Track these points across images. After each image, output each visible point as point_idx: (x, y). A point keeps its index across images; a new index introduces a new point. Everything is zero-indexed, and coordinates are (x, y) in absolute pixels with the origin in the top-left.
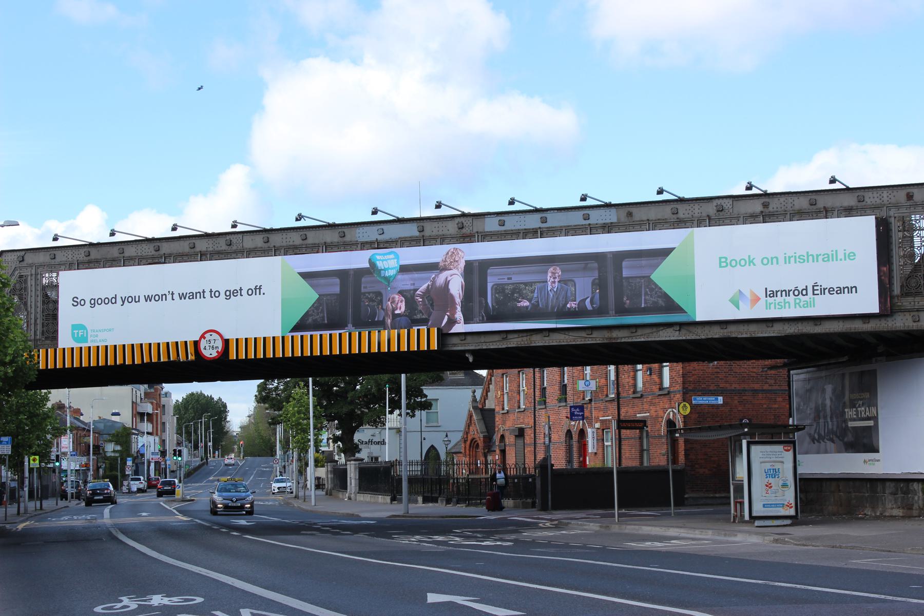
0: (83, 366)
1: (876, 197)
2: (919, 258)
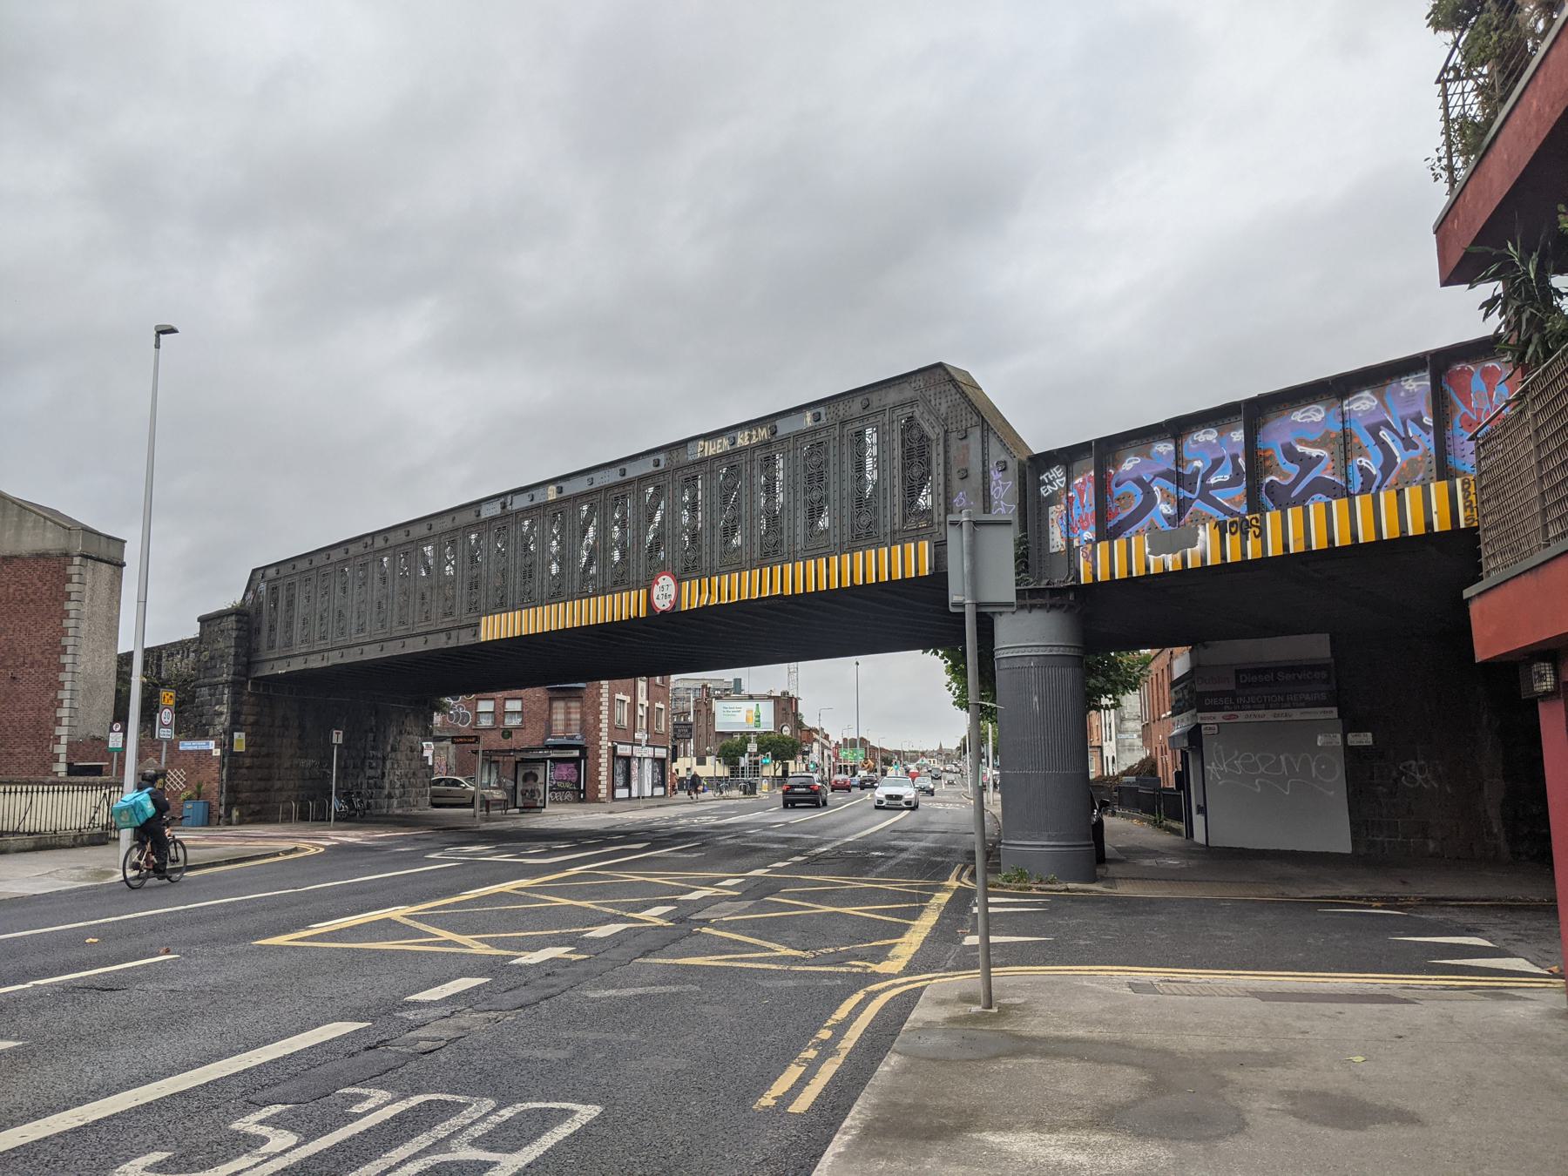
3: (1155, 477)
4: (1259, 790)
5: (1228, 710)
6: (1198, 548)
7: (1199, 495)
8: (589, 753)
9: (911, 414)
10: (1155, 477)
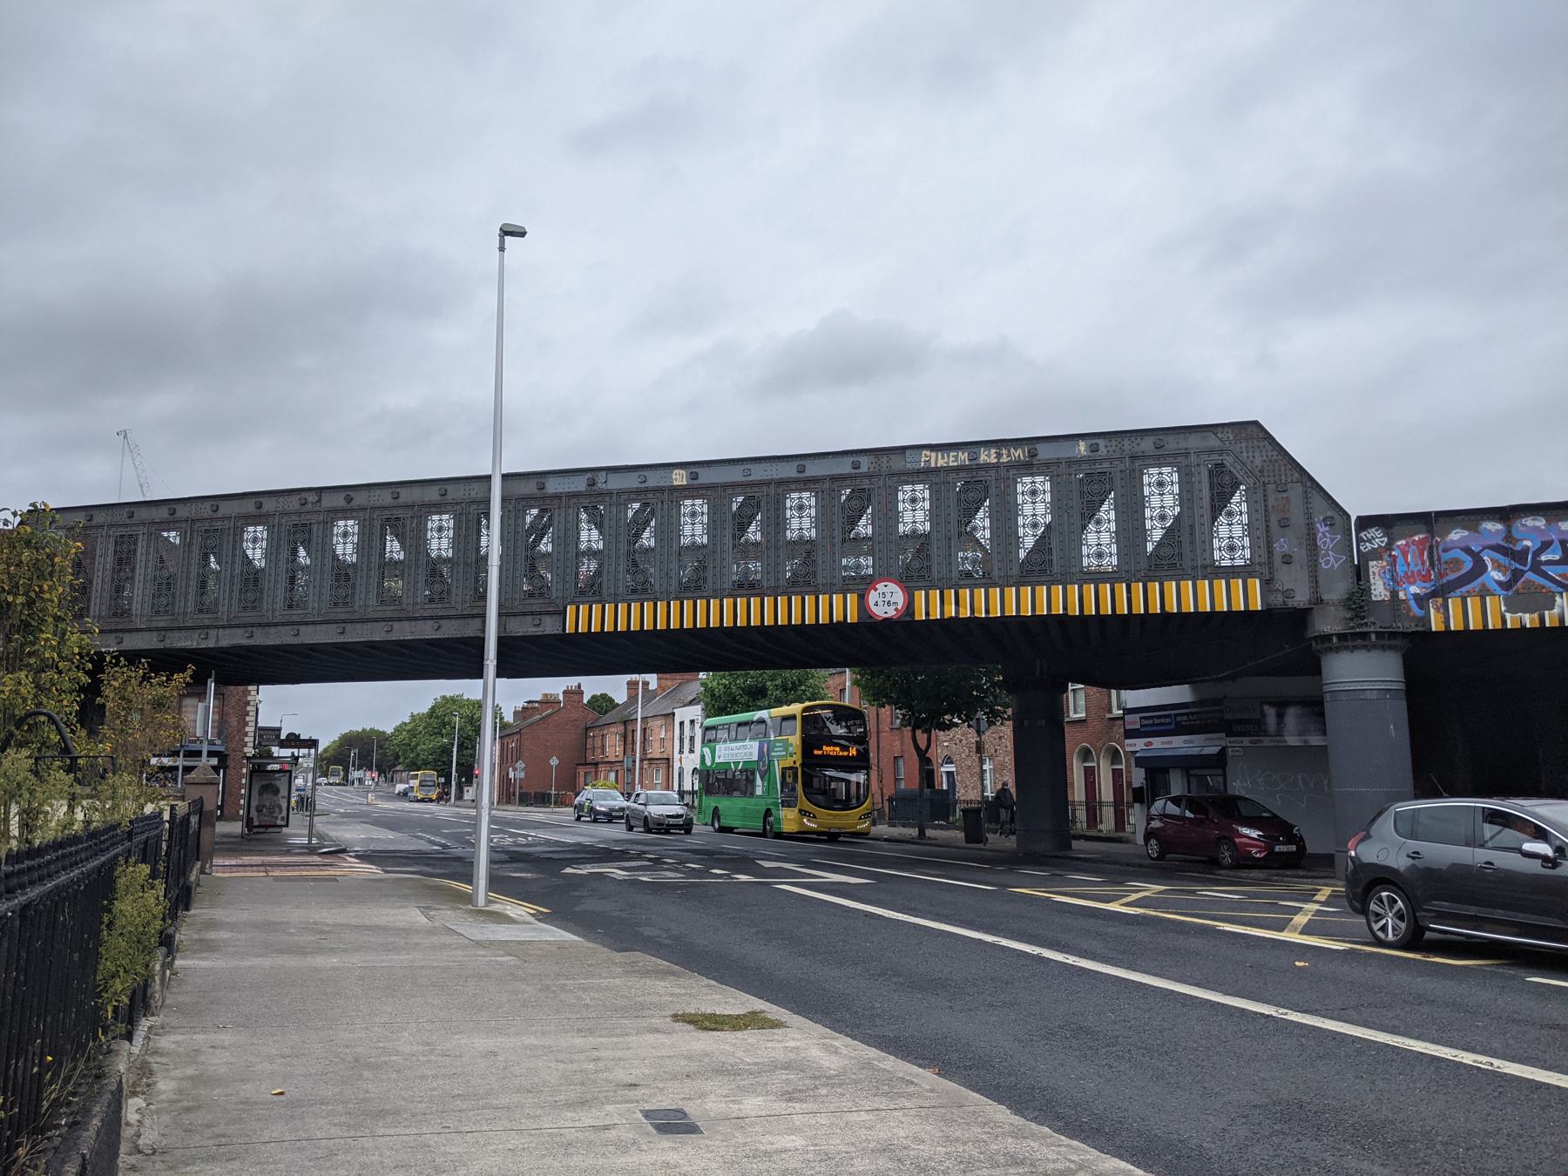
0: (711, 626)
1: (1114, 445)
2: (1172, 521)
3: (1484, 548)
4: (1279, 803)
5: (1253, 736)
6: (1556, 611)
7: (1531, 566)
8: (230, 762)
9: (1220, 462)
10: (1484, 548)
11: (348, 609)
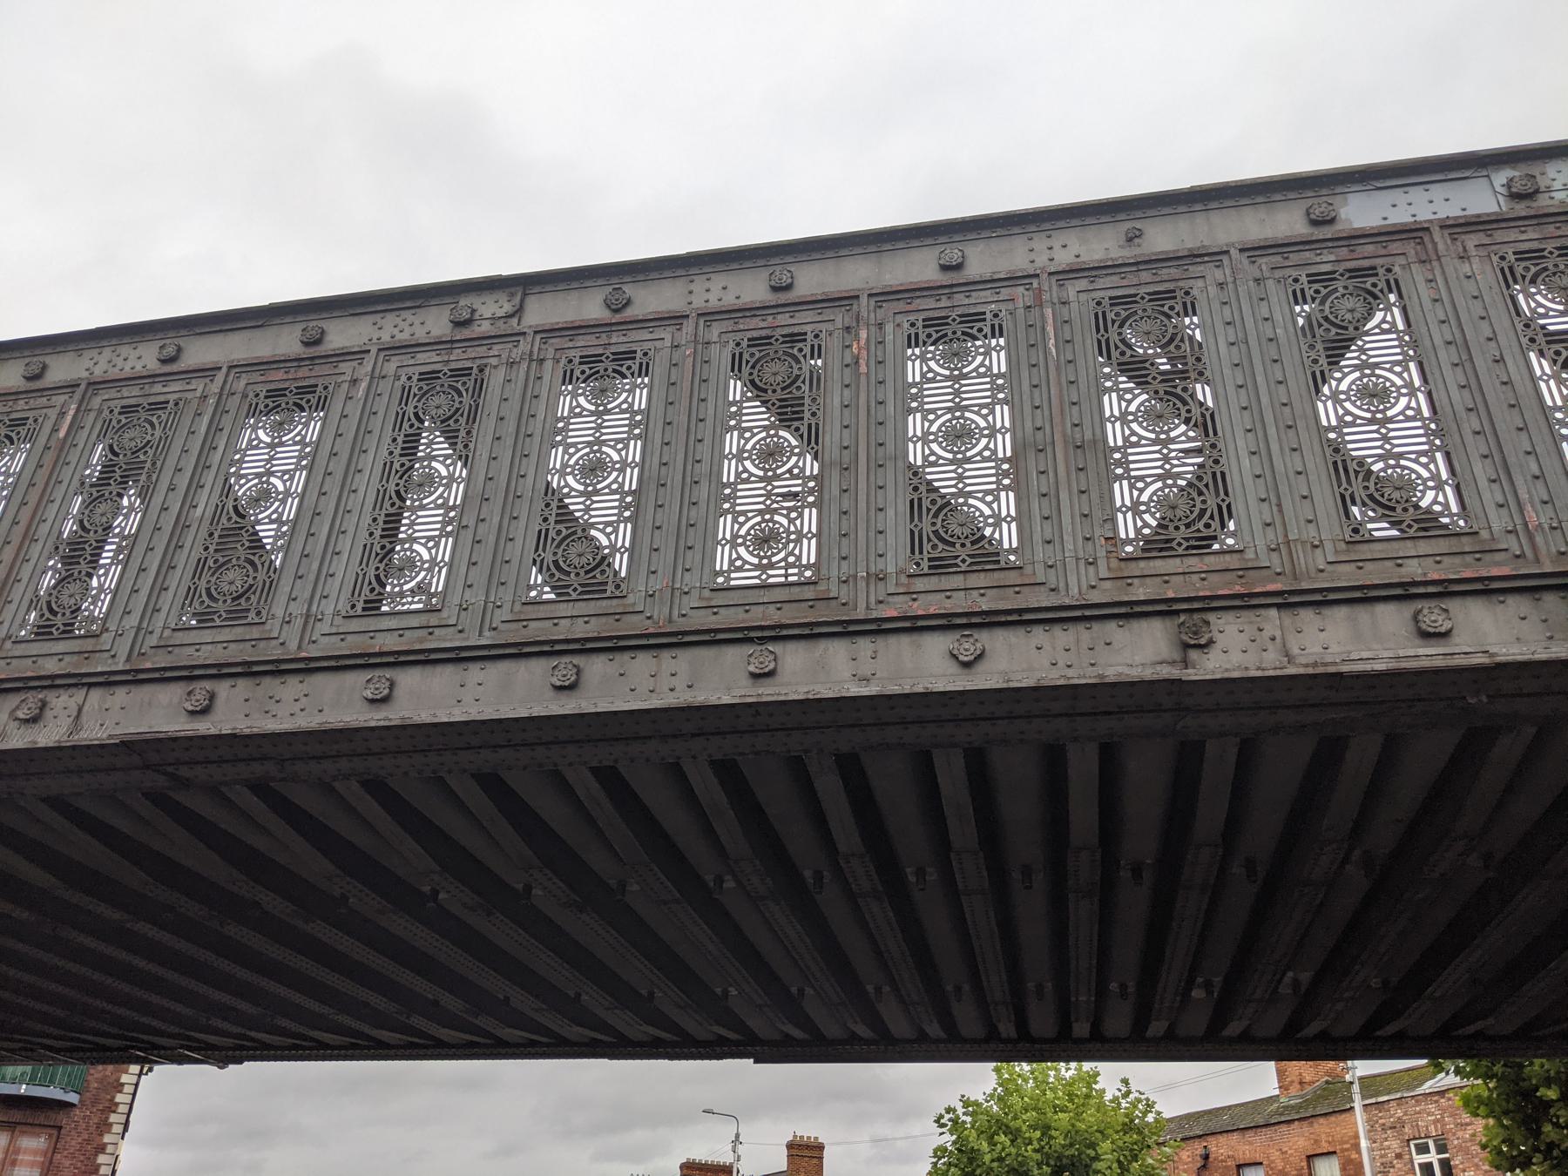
11: (603, 606)
